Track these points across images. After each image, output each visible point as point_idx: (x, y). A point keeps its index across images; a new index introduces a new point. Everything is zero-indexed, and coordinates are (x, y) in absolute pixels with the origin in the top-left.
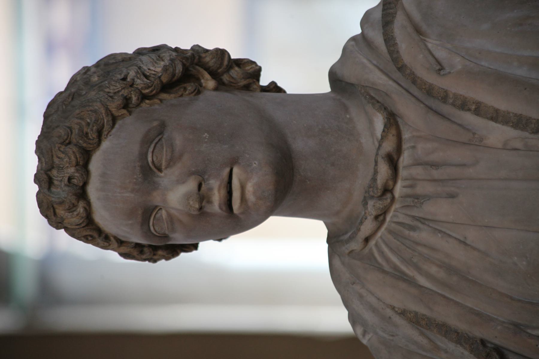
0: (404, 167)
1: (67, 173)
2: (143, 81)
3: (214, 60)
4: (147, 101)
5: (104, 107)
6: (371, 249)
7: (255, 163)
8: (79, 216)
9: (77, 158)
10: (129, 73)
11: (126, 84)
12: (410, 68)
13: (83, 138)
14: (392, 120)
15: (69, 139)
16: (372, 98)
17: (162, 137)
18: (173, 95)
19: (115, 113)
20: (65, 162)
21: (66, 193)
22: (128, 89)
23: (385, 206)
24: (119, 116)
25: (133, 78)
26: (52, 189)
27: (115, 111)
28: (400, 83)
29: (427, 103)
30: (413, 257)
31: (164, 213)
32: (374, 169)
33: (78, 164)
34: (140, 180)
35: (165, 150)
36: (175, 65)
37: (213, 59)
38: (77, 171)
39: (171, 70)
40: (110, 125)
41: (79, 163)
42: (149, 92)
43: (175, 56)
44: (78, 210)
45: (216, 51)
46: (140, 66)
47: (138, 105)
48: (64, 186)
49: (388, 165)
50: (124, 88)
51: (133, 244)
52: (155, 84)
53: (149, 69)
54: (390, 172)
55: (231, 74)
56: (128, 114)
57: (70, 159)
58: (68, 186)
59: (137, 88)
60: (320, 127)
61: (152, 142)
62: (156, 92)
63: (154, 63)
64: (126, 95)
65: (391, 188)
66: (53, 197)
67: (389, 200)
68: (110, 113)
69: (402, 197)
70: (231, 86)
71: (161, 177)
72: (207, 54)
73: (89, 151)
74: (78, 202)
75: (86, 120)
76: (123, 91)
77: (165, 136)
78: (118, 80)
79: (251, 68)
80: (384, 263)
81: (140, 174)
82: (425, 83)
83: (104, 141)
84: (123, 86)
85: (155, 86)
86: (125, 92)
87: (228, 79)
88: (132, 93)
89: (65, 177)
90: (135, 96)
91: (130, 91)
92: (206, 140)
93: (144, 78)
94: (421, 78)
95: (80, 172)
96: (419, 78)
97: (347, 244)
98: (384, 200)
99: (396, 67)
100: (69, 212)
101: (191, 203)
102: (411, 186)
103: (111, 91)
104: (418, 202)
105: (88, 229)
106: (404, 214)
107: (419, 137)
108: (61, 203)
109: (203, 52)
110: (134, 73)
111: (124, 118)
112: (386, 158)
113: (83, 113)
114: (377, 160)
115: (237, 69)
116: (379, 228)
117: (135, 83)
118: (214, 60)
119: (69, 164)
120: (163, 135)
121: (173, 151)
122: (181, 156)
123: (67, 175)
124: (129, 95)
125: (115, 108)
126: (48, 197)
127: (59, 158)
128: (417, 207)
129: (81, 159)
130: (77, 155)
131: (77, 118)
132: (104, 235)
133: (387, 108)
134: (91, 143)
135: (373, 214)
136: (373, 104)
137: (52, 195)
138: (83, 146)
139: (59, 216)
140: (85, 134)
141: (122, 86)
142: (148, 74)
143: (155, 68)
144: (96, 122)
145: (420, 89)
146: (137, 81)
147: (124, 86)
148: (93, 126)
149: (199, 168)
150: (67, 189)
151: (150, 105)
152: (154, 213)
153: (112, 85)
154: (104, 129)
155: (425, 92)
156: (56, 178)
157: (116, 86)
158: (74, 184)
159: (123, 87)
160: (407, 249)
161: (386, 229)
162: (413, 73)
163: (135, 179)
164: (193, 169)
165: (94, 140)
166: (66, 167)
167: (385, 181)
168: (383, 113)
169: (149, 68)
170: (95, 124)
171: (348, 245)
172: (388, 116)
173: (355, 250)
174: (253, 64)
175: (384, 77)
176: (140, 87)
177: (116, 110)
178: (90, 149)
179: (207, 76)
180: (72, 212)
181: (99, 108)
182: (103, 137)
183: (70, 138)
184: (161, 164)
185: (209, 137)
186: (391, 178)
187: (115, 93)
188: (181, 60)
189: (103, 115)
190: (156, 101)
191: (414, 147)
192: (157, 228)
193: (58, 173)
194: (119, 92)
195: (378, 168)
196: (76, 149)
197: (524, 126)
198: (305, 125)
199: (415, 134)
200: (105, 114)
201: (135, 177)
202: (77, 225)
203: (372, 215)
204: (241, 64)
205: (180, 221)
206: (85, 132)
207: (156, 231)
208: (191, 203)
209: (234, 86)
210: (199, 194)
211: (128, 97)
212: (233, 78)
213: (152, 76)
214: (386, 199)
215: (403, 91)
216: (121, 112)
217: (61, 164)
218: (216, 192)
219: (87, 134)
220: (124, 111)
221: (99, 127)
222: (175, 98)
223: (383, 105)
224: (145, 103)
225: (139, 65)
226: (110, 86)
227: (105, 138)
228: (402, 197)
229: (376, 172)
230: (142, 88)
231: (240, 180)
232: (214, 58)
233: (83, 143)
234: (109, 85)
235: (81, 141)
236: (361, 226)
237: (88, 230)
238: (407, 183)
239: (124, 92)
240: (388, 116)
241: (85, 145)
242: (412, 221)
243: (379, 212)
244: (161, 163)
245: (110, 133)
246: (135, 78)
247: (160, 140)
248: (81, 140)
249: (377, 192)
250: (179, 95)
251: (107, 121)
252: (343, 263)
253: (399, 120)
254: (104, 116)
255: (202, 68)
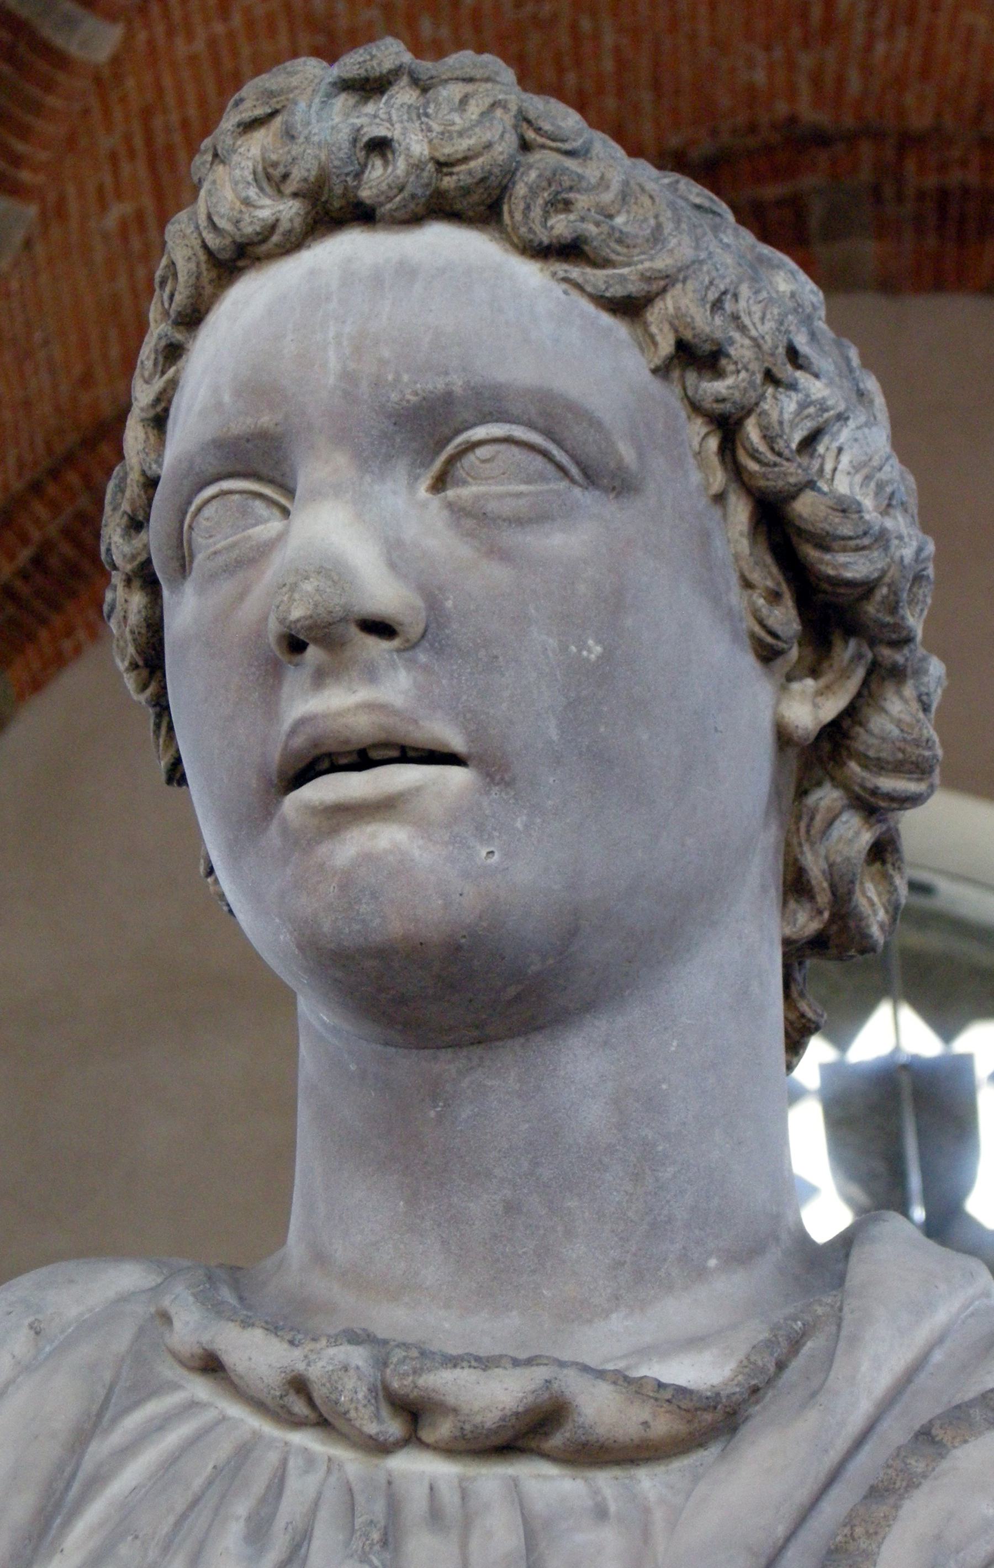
0: (515, 1483)
1: (404, 128)
2: (793, 425)
3: (896, 732)
4: (713, 443)
5: (680, 270)
6: (174, 1386)
7: (491, 853)
8: (243, 208)
9: (465, 159)
10: (817, 376)
11: (772, 355)
12: (934, 1469)
13: (550, 185)
14: (708, 1417)
15: (540, 140)
16: (796, 1344)
17: (573, 481)
18: (744, 545)
19: (656, 310)
20: (448, 117)
21: (328, 138)
22: (757, 359)
23: (346, 1413)
24: (646, 326)
25: (801, 386)
26: (343, 96)
27: (667, 309)
28: (867, 1448)
29: (790, 1553)
30: (138, 1542)
31: (275, 525)
32: (501, 1356)
33: (445, 170)
34: (394, 396)
35: (523, 488)
36: (864, 548)
37: (898, 726)
38: (418, 167)
39: (846, 530)
40: (607, 289)
41: (446, 175)
42: (752, 443)
43: (898, 554)
44: (267, 202)
45: (928, 741)
46: (847, 419)
47: (695, 407)
48: (353, 124)
49: (521, 1409)
50: (758, 346)
51: (154, 466)
52: (785, 463)
53: (840, 450)
54: (490, 1419)
55: (844, 817)
56: (657, 361)
57: (461, 134)
58: (355, 141)
59: (762, 397)
60: (660, 1148)
61: (548, 434)
62: (756, 472)
63: (865, 471)
64: (732, 351)
65: (427, 1435)
66: (310, 106)
67: (372, 1428)
68: (655, 287)
69: (390, 1483)
70: (799, 818)
71: (412, 487)
72: (915, 706)
73: (499, 214)
74: (295, 195)
75: (619, 212)
76: (747, 342)
77: (577, 491)
78: (788, 332)
79: (872, 904)
80: (134, 1421)
81: (416, 394)
82: (876, 1533)
83: (542, 270)
84: (765, 342)
85: (775, 465)
86: (740, 349)
87: (823, 804)
88: (743, 374)
89: (388, 125)
90: (729, 388)
91: (751, 367)
92: (573, 649)
93: (802, 429)
94: (895, 1519)
95: (412, 178)
96: (897, 1507)
97: (194, 1295)
98: (373, 1408)
99: (931, 1421)
100: (255, 173)
101: (308, 587)
102: (435, 1515)
103: (742, 304)
104: (372, 1545)
105: (198, 264)
106: (319, 1495)
107: (646, 1535)
108: (289, 135)
109: (924, 689)
110: (819, 395)
111: (642, 350)
112: (546, 1396)
113: (647, 201)
114: (538, 1365)
115: (867, 838)
116: (259, 1405)
117: (781, 390)
118: (896, 732)
119: (443, 133)
120: (581, 486)
121: (519, 521)
122: (503, 555)
123: (395, 133)
124: (731, 368)
125: (677, 309)
126: (309, 90)
127: (464, 101)
128: (347, 1543)
129: (462, 177)
130: (480, 160)
131: (626, 183)
132: (179, 337)
133: (757, 1402)
134: (532, 215)
135: (310, 1369)
136: (769, 1344)
137: (317, 100)
138: (514, 184)
139: (239, 142)
140: (565, 195)
141: (767, 337)
142: (821, 449)
143: (849, 473)
144: (617, 235)
145: (850, 1521)
146: (790, 397)
147: (767, 347)
148: (597, 224)
149: (455, 626)
150: (344, 135)
151: (699, 453)
152: (267, 491)
153: (766, 308)
154: (588, 270)
155: (839, 1538)
156: (385, 104)
157: (763, 319)
158: (364, 167)
159: (761, 342)
160: (171, 1519)
161: (257, 1436)
162: (912, 1484)
163: (397, 379)
164: (449, 604)
165: (543, 230)
166: (427, 124)
167: (451, 1400)
168: (735, 1382)
169: (845, 447)
170: (605, 228)
171: (191, 1299)
172: (724, 1400)
173: (171, 1330)
174: (887, 912)
175: (883, 1381)
176: (766, 407)
177: (671, 310)
178: (506, 217)
179: (831, 708)
180: (256, 180)
181: (671, 251)
182: (562, 268)
183: (543, 147)
184: (465, 483)
185: (587, 660)
186: (468, 1427)
187: (736, 318)
188: (887, 580)
189: (647, 265)
190: (719, 478)
191: (601, 1513)
192: (208, 511)
193: (406, 107)
194: (743, 329)
195: (505, 1368)
196: (502, 153)
197: (460, 675)
198: (664, 1086)
199: (658, 1516)
200: (651, 268)
201: (406, 378)
202: (210, 217)
203: (309, 1365)
204: (884, 862)
205: (242, 596)
206: (571, 196)
207: (199, 510)
208: (308, 587)
209: (798, 829)
210: (344, 620)
211: (724, 362)
212: (830, 823)
213: (816, 464)
214: (377, 1417)
215: (833, 1456)
216: (661, 330)
217: (438, 105)
218: (363, 694)
219: (567, 206)
220: (666, 346)
221: (595, 243)
222: (737, 557)
223: (770, 1382)
224: (707, 435)
225: (852, 416)
226: (763, 304)
227: (554, 274)
228: (390, 1483)
229: (485, 1363)
230: (764, 413)
231: (416, 791)
232: (902, 731)
233: (526, 184)
234: (764, 299)
235: (533, 175)
236: (262, 1327)
237: (192, 266)
238: (450, 1498)
239: (742, 346)
240: (724, 1400)
241: (521, 189)
242: (290, 1527)
243: (319, 1393)
244: (469, 479)
245: (575, 295)
246: (800, 396)
247: (560, 468)
248: (539, 176)
249: (405, 1375)
250: (747, 574)
251: (621, 275)
252: (124, 1298)
253: (713, 1450)
254: (640, 267)
255: (859, 695)
